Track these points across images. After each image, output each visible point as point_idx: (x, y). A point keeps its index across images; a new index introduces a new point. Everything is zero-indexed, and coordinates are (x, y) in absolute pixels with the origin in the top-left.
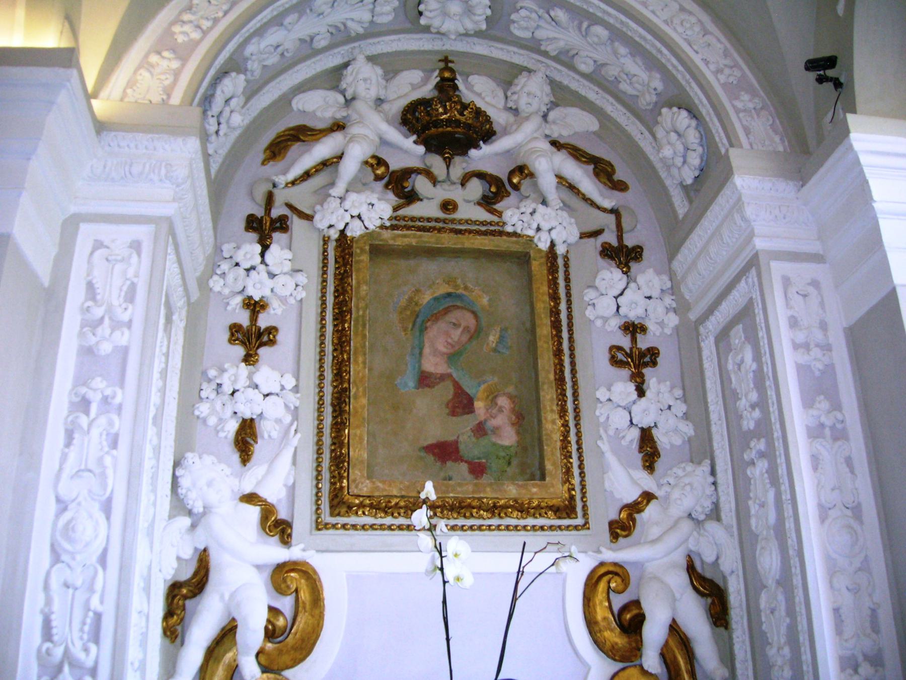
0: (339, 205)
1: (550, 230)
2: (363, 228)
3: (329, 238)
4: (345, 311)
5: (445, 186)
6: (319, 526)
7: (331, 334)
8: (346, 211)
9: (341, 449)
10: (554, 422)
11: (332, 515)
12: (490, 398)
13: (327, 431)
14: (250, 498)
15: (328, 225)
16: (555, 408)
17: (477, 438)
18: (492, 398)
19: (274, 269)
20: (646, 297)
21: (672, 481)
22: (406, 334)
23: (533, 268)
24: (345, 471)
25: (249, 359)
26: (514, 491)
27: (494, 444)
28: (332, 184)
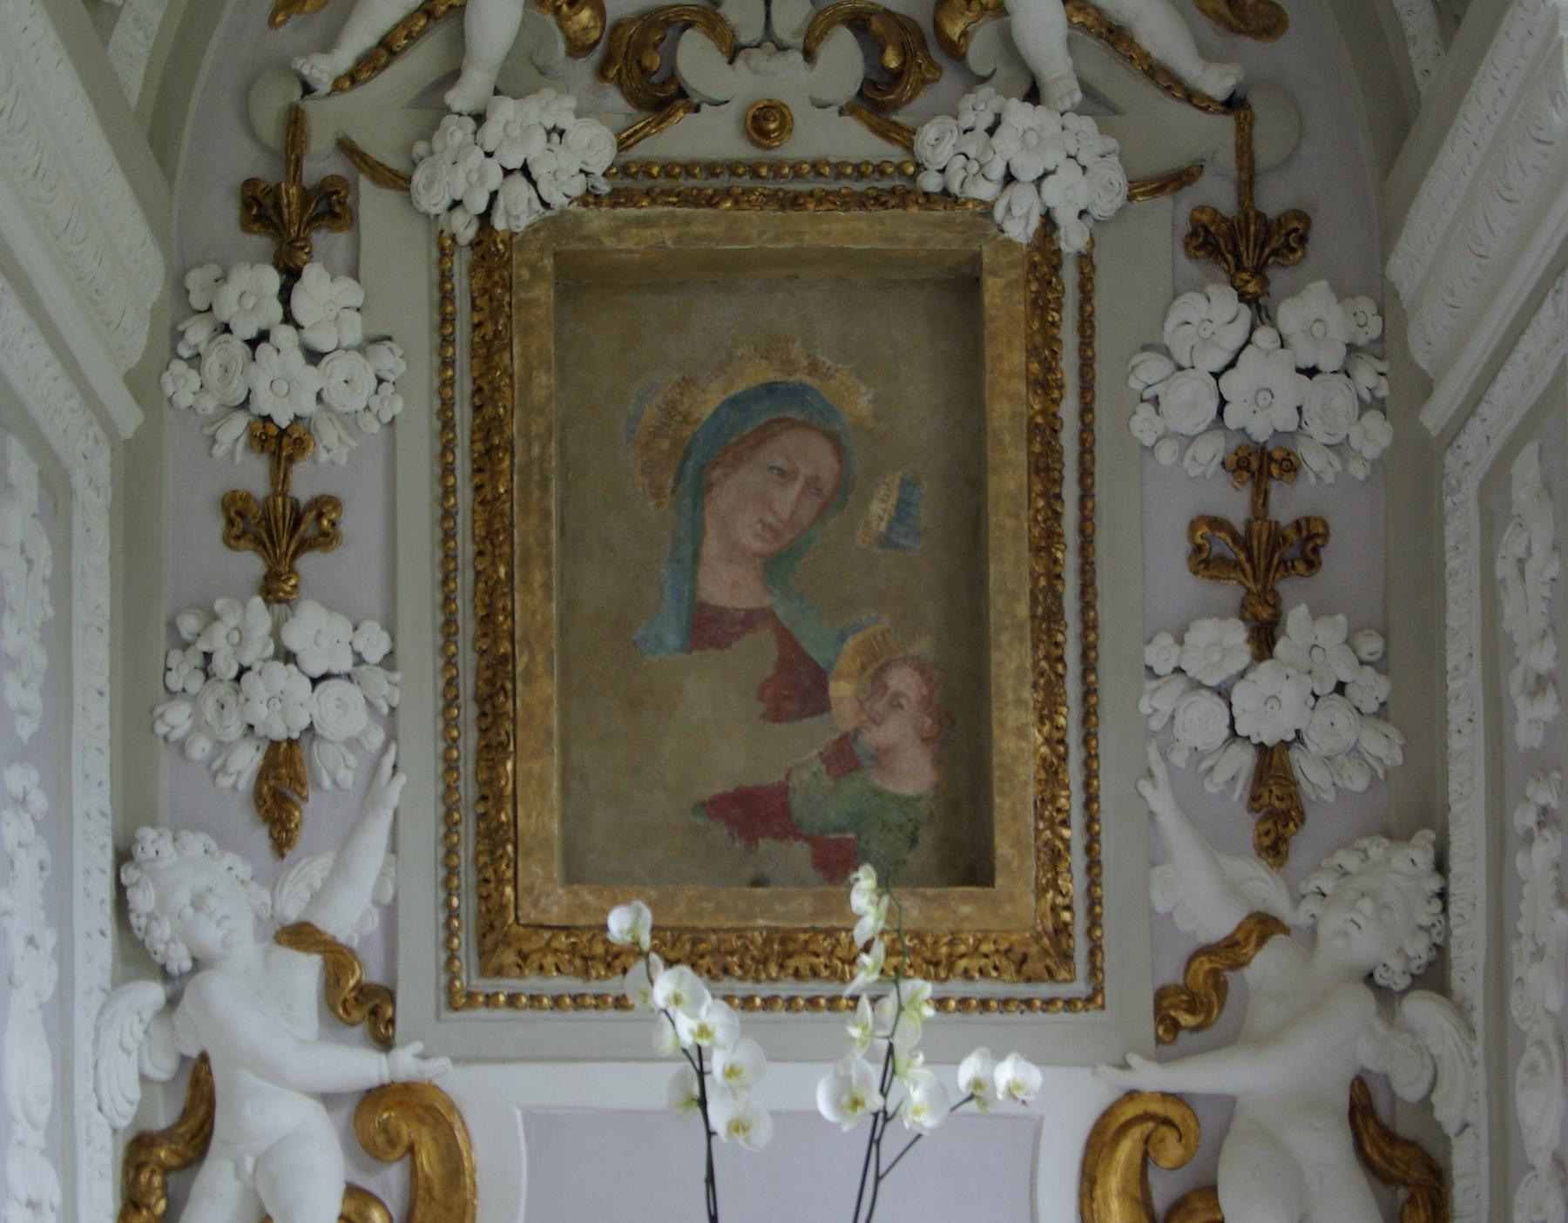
0: (470, 138)
1: (1039, 182)
2: (537, 205)
3: (453, 238)
4: (498, 447)
5: (759, 58)
6: (456, 999)
7: (469, 514)
8: (489, 155)
9: (499, 811)
10: (1021, 734)
11: (483, 972)
12: (870, 671)
13: (468, 767)
14: (299, 935)
15: (447, 202)
16: (1027, 694)
17: (836, 778)
18: (875, 673)
19: (322, 342)
20: (1299, 371)
21: (1327, 885)
22: (659, 505)
23: (987, 299)
24: (508, 866)
25: (275, 589)
26: (914, 912)
27: (878, 793)
28: (453, 77)
